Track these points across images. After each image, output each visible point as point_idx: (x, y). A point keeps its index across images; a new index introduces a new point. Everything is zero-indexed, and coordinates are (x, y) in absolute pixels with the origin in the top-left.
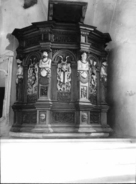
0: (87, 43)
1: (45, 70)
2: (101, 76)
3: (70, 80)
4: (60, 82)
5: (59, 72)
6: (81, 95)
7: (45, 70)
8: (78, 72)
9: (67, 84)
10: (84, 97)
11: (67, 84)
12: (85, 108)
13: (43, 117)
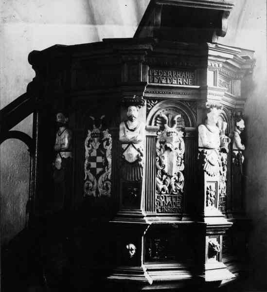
0: (218, 87)
1: (135, 148)
2: (235, 154)
3: (182, 168)
4: (163, 173)
5: (160, 150)
6: (207, 202)
7: (135, 148)
8: (200, 152)
9: (177, 178)
10: (212, 204)
11: (177, 178)
12: (216, 230)
13: (132, 250)
